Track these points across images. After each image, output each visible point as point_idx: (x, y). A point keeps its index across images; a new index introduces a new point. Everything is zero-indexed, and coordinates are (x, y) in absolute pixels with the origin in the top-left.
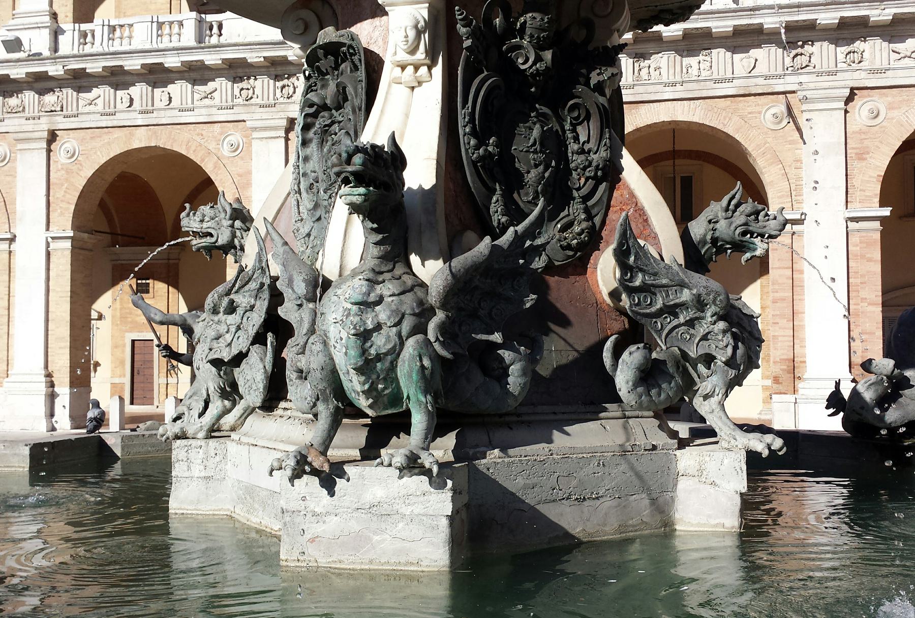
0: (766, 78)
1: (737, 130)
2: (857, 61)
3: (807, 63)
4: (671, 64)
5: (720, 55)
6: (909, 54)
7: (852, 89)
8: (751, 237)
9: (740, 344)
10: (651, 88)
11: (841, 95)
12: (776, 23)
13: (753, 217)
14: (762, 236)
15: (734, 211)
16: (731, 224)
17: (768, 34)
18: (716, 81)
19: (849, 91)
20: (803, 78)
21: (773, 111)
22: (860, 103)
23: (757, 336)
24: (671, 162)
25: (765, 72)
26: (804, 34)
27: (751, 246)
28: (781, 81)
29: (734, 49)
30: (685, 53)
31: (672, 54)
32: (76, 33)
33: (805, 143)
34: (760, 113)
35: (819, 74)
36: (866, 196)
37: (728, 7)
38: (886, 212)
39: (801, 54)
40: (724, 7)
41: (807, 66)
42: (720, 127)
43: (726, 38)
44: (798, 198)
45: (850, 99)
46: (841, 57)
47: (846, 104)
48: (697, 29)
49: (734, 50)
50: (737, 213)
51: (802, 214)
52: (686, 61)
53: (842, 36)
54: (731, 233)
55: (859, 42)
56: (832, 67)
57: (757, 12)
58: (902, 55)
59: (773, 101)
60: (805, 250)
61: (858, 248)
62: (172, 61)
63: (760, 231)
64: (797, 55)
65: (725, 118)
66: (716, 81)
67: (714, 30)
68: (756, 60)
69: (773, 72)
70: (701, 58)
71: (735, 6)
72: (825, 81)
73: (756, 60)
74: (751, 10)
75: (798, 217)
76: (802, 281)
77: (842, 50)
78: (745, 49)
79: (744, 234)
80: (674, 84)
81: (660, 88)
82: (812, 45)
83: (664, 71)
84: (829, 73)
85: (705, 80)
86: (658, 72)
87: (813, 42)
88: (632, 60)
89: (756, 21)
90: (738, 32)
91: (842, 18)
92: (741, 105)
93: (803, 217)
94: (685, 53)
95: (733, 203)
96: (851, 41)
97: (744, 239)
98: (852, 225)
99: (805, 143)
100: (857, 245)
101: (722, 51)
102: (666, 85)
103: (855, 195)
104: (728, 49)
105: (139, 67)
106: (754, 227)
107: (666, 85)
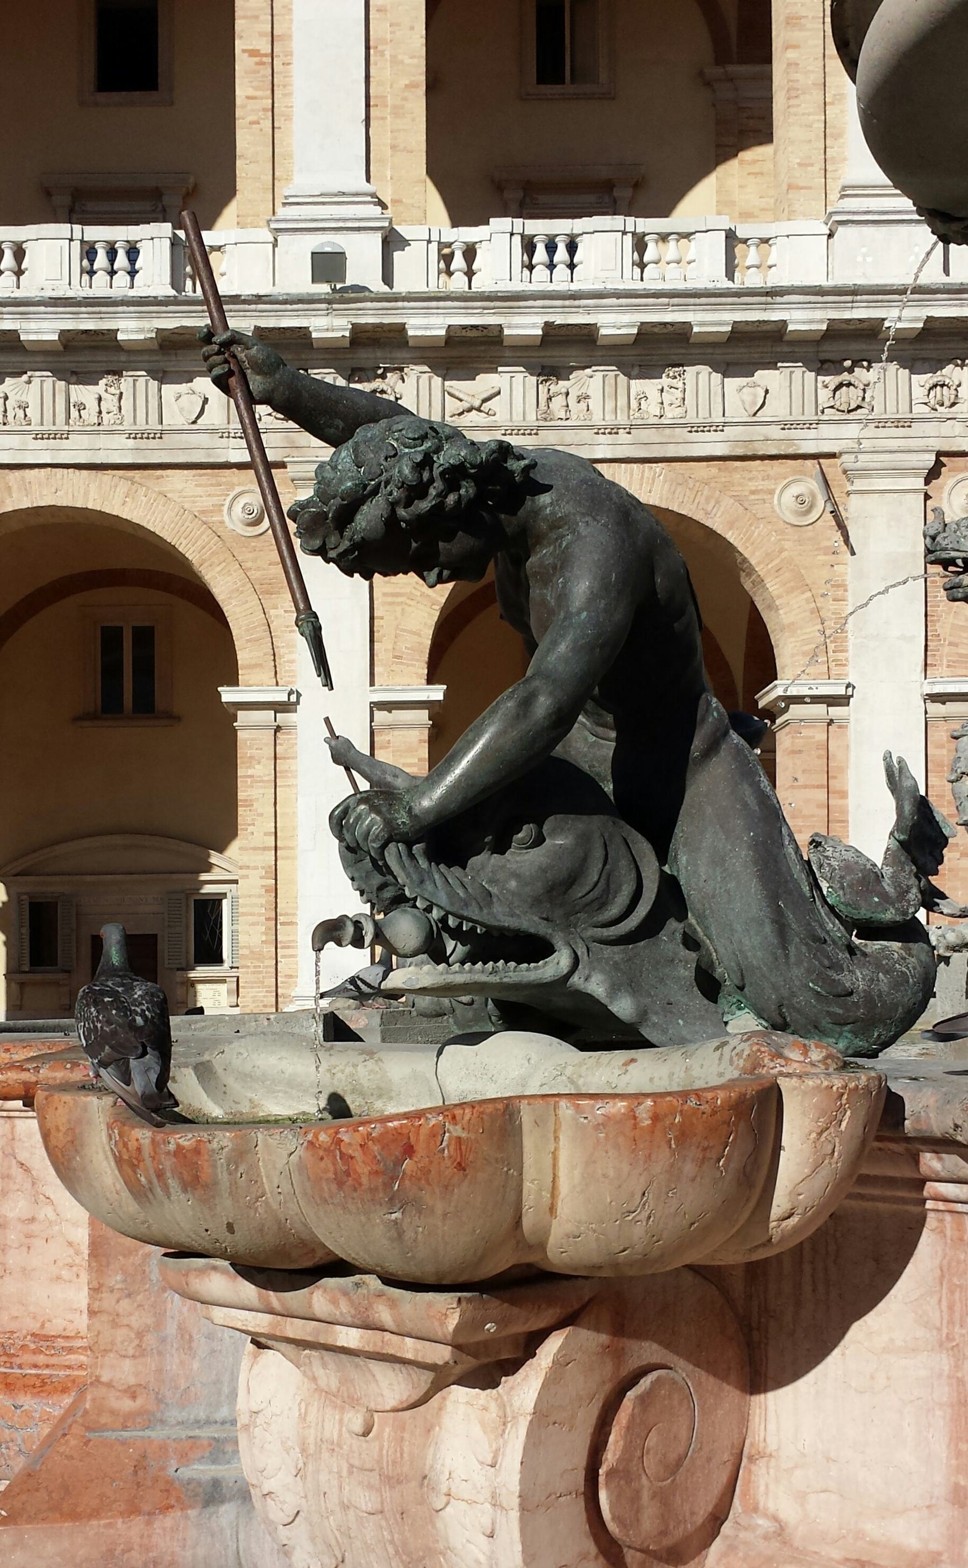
0: (786, 425)
1: (731, 525)
2: (947, 403)
3: (859, 402)
6: (477, 403)
7: (939, 454)
10: (569, 436)
11: (921, 465)
12: (821, 321)
17: (791, 343)
19: (933, 457)
20: (853, 430)
21: (795, 490)
22: (951, 482)
26: (856, 347)
28: (812, 434)
29: (728, 369)
30: (636, 371)
31: (611, 371)
32: (76, 245)
33: (853, 553)
34: (771, 492)
35: (881, 423)
36: (961, 655)
38: (437, 693)
39: (849, 385)
40: (710, 286)
42: (699, 516)
43: (150, 351)
44: (840, 656)
45: (933, 474)
46: (919, 393)
47: (927, 482)
48: (665, 324)
51: (848, 686)
52: (638, 385)
53: (925, 354)
55: (951, 366)
56: (904, 413)
57: (778, 299)
58: (466, 405)
59: (795, 472)
60: (852, 754)
62: (131, 329)
64: (840, 386)
65: (708, 500)
67: (314, 335)
68: (767, 392)
69: (797, 416)
70: (665, 381)
71: (386, 289)
72: (891, 438)
73: (767, 392)
74: (767, 294)
75: (841, 691)
76: (844, 811)
77: (922, 380)
80: (614, 430)
81: (682, 433)
83: (595, 403)
84: (899, 423)
85: (111, 432)
86: (583, 405)
87: (870, 362)
88: (534, 379)
89: (775, 316)
90: (742, 336)
91: (929, 319)
92: (737, 476)
93: (293, 698)
96: (936, 365)
98: (380, 716)
99: (853, 553)
100: (942, 747)
102: (599, 431)
103: (943, 653)
104: (531, 370)
105: (55, 337)
107: (599, 431)
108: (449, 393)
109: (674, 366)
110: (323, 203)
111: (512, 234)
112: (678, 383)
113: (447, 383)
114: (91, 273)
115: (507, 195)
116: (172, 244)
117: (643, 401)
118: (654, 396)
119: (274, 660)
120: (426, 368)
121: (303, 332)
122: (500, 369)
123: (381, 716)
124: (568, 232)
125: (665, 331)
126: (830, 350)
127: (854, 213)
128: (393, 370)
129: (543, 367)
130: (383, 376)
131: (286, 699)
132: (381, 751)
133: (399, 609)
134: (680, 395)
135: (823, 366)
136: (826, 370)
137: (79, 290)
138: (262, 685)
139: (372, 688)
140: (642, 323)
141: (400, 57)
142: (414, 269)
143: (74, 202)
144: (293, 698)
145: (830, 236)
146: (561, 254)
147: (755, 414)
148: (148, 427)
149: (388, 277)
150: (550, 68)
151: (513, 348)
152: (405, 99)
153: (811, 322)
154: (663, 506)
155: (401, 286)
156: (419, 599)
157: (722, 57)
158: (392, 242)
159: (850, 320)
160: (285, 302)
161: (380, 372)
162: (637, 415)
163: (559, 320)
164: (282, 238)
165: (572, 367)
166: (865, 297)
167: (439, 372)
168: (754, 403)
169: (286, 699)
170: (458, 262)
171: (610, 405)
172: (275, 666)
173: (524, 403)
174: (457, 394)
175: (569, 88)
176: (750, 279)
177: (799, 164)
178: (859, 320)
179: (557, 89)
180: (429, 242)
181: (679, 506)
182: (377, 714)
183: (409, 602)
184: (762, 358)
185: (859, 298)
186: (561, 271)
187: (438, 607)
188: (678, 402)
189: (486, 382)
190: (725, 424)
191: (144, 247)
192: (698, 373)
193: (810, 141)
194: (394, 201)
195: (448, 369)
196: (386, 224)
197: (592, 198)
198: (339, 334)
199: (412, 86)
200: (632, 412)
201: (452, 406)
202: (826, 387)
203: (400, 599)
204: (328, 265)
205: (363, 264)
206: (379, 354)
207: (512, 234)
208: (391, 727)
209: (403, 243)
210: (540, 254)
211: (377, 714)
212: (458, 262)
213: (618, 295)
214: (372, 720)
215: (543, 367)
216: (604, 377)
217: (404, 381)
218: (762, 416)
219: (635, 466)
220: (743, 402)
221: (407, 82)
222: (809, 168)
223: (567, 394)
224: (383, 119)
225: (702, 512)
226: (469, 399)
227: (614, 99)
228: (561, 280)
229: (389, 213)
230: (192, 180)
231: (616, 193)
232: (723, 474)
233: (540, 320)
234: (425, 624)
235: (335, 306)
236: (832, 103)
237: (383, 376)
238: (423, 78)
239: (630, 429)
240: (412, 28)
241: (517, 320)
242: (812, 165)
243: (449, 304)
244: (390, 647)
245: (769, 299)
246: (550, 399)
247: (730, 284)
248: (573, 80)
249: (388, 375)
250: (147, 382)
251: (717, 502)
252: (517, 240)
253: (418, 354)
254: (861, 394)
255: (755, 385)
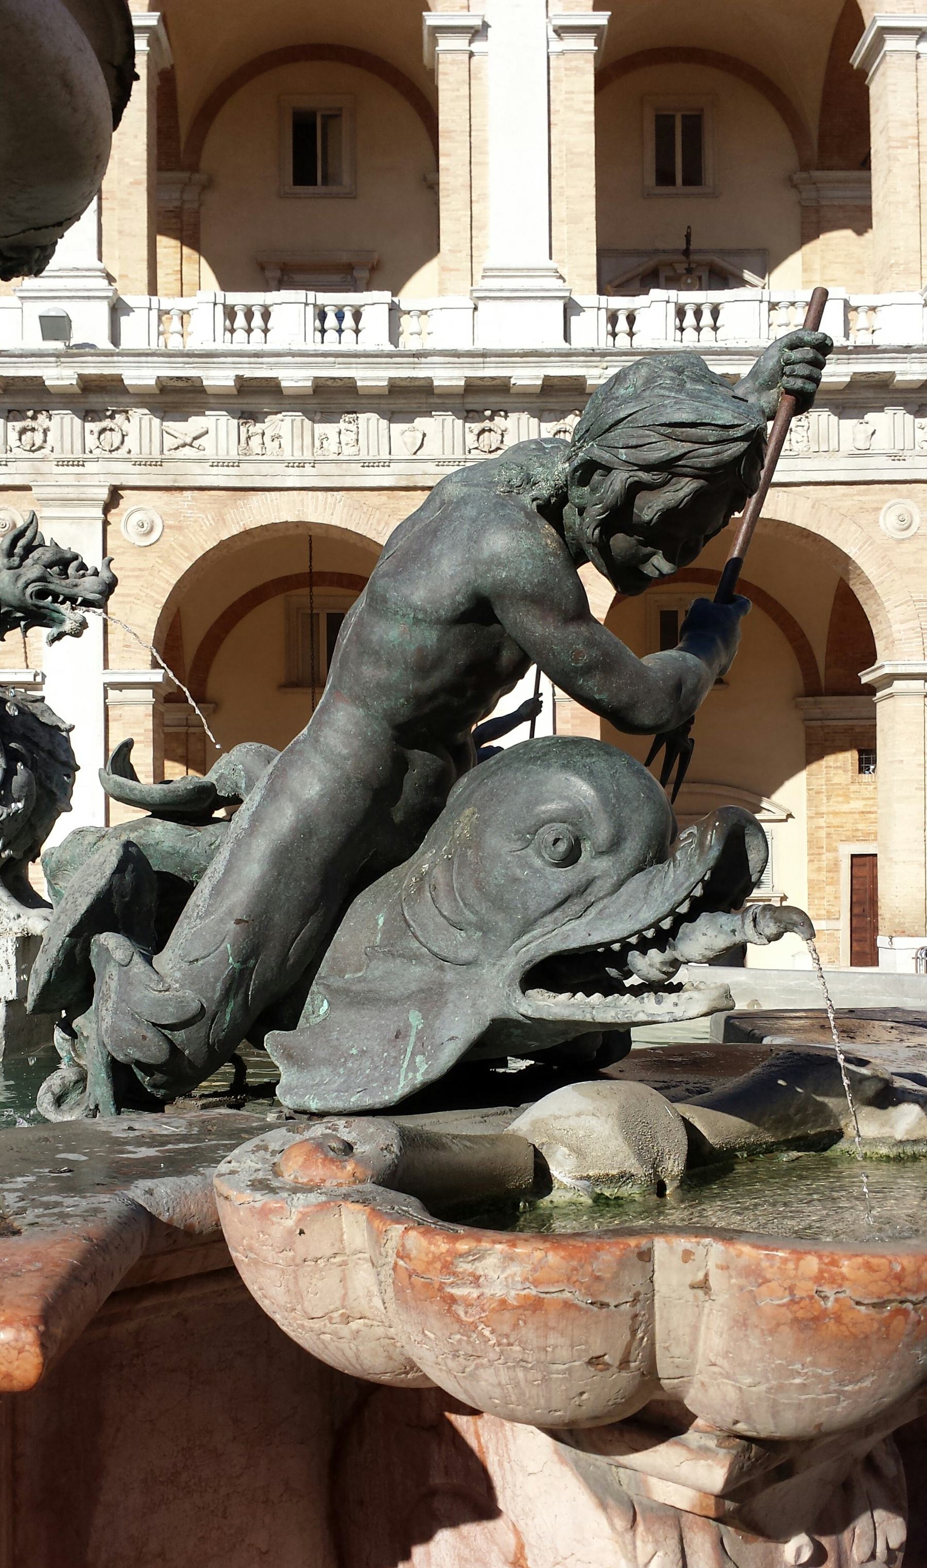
3: (497, 444)
4: (297, 431)
5: (369, 422)
6: (188, 440)
8: (55, 600)
9: (20, 766)
10: (265, 468)
12: (459, 378)
13: (56, 569)
14: (73, 600)
15: (24, 558)
16: (18, 577)
17: (440, 396)
18: (366, 464)
23: (63, 757)
24: (306, 591)
25: (437, 454)
26: (493, 399)
27: (55, 615)
30: (318, 417)
31: (298, 417)
37: (381, 348)
39: (490, 430)
40: (375, 348)
41: (498, 449)
43: (380, 396)
49: (392, 416)
50: (29, 562)
52: (320, 428)
53: (551, 406)
54: (17, 592)
57: (423, 360)
58: (180, 442)
61: (569, 726)
63: (67, 591)
64: (483, 431)
65: (379, 523)
66: (366, 464)
68: (424, 435)
70: (342, 425)
71: (392, 348)
73: (424, 435)
74: (414, 356)
78: (407, 416)
79: (41, 594)
80: (302, 465)
81: (279, 468)
82: (506, 417)
83: (286, 441)
85: (348, 461)
86: (276, 442)
87: (506, 412)
88: (236, 421)
90: (397, 389)
91: (547, 378)
94: (318, 417)
95: (21, 543)
97: (42, 603)
100: (568, 722)
101: (374, 417)
104: (232, 413)
105: (153, 382)
106: (58, 584)
108: (167, 432)
109: (348, 413)
110: (61, 277)
111: (215, 304)
112: (352, 427)
113: (165, 423)
114: (232, 331)
115: (268, 274)
116: (390, 310)
117: (324, 441)
118: (334, 437)
119: (25, 647)
120: (147, 411)
121: (39, 381)
122: (207, 413)
123: (113, 694)
124: (262, 303)
125: (335, 384)
126: (473, 402)
127: (490, 290)
128: (120, 412)
129: (243, 413)
130: (112, 417)
131: (32, 680)
132: (115, 723)
133: (128, 606)
134: (355, 437)
135: (469, 414)
136: (472, 418)
137: (313, 344)
138: (14, 668)
139: (107, 671)
140: (855, 373)
141: (126, 160)
142: (134, 331)
143: (283, 275)
144: (39, 679)
145: (476, 309)
146: (257, 321)
147: (415, 453)
148: (72, 456)
149: (115, 338)
150: (305, 172)
151: (216, 396)
152: (130, 194)
153: (451, 379)
154: (343, 526)
155: (126, 343)
156: (144, 599)
157: (805, 167)
158: (118, 309)
159: (484, 378)
160: (21, 356)
161: (108, 413)
162: (320, 452)
163: (248, 374)
164: (481, 304)
165: (266, 412)
166: (493, 359)
167: (157, 414)
168: (415, 444)
169: (32, 680)
170: (622, 325)
171: (297, 443)
172: (26, 653)
173: (228, 441)
174: (172, 432)
175: (319, 189)
176: (408, 343)
177: (450, 251)
178: (491, 378)
179: (310, 189)
180: (150, 309)
181: (356, 526)
182: (111, 693)
183: (135, 601)
184: (419, 407)
185: (488, 360)
186: (257, 335)
187: (160, 606)
188: (353, 442)
189: (196, 424)
190: (390, 461)
191: (365, 312)
192: (368, 420)
193: (458, 232)
194: (121, 276)
195: (165, 412)
196: (567, 294)
197: (336, 278)
198: (67, 382)
199: (136, 183)
200: (315, 450)
201: (169, 442)
202: (471, 432)
203: (129, 599)
204: (56, 327)
205: (90, 324)
206: (107, 399)
207: (215, 304)
208: (122, 703)
209: (128, 310)
210: (240, 321)
211: (111, 693)
212: (622, 325)
213: (293, 354)
214: (106, 697)
215: (243, 413)
216: (293, 421)
217: (129, 421)
218: (421, 455)
219: (319, 493)
220: (405, 443)
221: (132, 180)
222: (459, 255)
223: (263, 434)
224: (113, 209)
225: (374, 532)
226: (182, 437)
227: (355, 198)
228: (257, 341)
229: (115, 285)
230: (376, 256)
231: (356, 274)
232: (391, 501)
233: (232, 373)
234: (149, 620)
235: (63, 359)
236: (477, 202)
237: (112, 417)
238: (145, 177)
239: (314, 464)
240: (136, 137)
241: (213, 373)
242: (461, 251)
243: (155, 359)
244: (121, 638)
245: (416, 359)
246: (249, 437)
247: (567, 346)
248: (325, 181)
249: (117, 416)
250: (72, 419)
251: (386, 524)
252: (219, 309)
253: (137, 400)
254: (500, 438)
255: (414, 430)
